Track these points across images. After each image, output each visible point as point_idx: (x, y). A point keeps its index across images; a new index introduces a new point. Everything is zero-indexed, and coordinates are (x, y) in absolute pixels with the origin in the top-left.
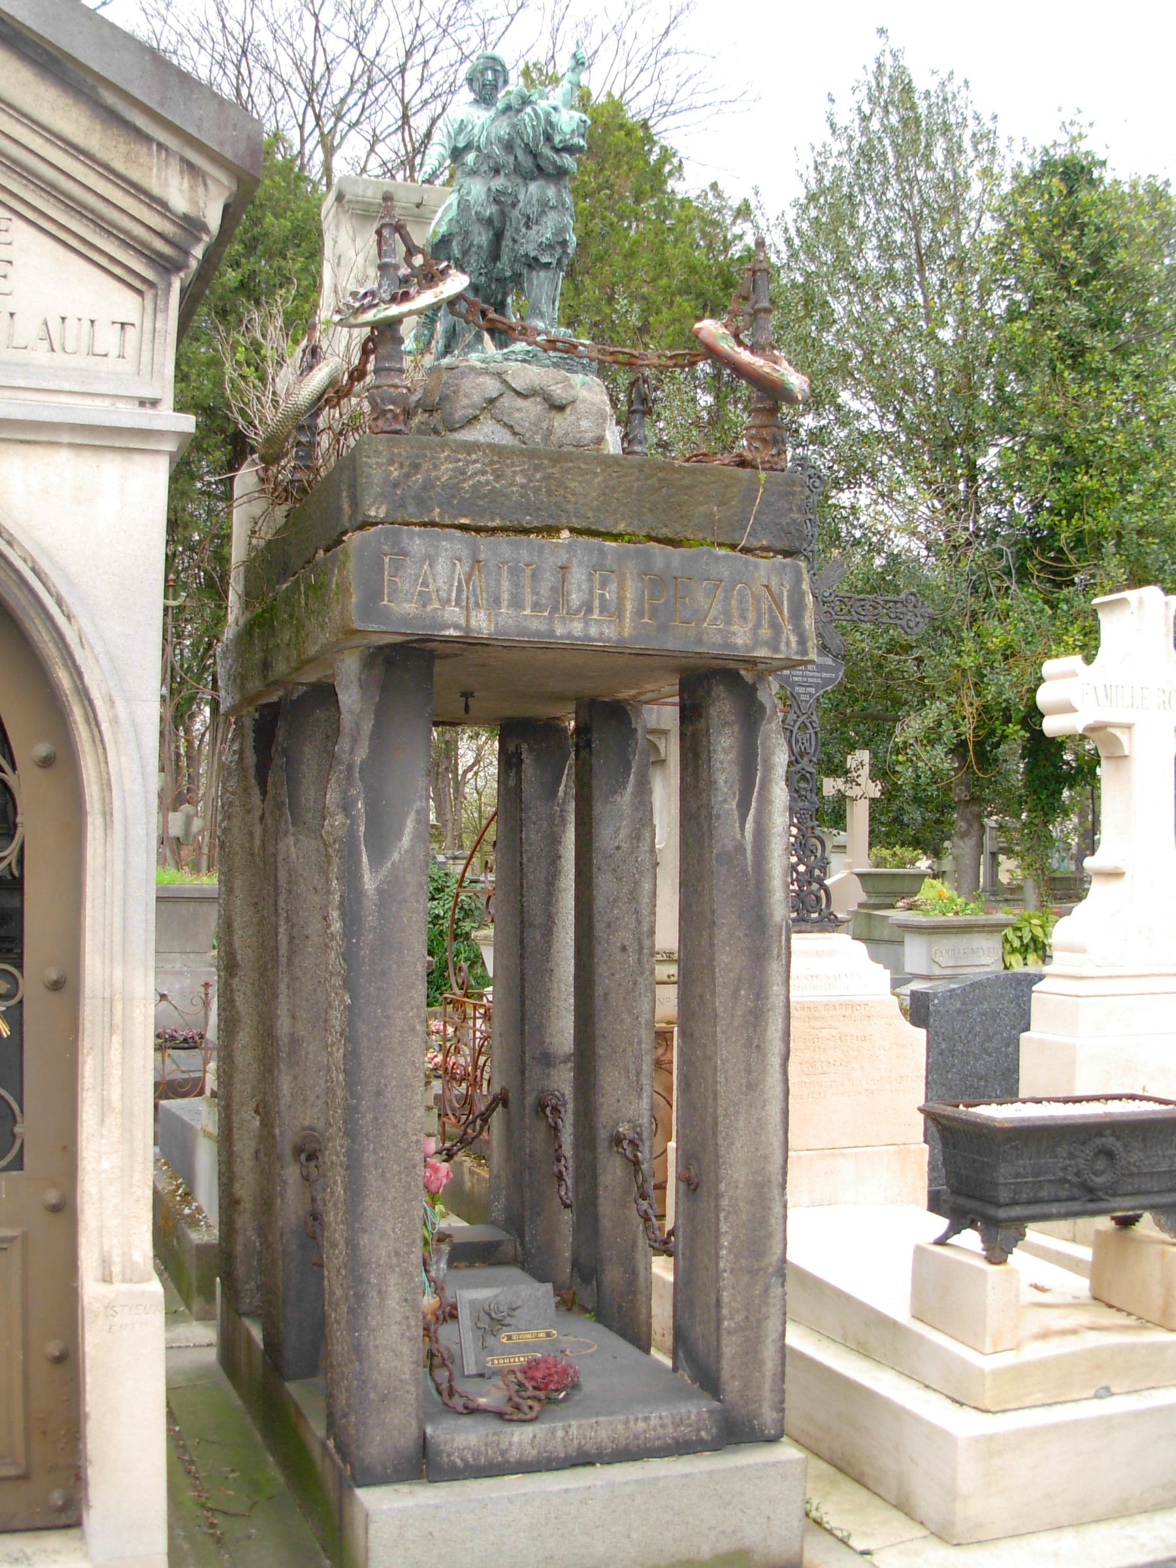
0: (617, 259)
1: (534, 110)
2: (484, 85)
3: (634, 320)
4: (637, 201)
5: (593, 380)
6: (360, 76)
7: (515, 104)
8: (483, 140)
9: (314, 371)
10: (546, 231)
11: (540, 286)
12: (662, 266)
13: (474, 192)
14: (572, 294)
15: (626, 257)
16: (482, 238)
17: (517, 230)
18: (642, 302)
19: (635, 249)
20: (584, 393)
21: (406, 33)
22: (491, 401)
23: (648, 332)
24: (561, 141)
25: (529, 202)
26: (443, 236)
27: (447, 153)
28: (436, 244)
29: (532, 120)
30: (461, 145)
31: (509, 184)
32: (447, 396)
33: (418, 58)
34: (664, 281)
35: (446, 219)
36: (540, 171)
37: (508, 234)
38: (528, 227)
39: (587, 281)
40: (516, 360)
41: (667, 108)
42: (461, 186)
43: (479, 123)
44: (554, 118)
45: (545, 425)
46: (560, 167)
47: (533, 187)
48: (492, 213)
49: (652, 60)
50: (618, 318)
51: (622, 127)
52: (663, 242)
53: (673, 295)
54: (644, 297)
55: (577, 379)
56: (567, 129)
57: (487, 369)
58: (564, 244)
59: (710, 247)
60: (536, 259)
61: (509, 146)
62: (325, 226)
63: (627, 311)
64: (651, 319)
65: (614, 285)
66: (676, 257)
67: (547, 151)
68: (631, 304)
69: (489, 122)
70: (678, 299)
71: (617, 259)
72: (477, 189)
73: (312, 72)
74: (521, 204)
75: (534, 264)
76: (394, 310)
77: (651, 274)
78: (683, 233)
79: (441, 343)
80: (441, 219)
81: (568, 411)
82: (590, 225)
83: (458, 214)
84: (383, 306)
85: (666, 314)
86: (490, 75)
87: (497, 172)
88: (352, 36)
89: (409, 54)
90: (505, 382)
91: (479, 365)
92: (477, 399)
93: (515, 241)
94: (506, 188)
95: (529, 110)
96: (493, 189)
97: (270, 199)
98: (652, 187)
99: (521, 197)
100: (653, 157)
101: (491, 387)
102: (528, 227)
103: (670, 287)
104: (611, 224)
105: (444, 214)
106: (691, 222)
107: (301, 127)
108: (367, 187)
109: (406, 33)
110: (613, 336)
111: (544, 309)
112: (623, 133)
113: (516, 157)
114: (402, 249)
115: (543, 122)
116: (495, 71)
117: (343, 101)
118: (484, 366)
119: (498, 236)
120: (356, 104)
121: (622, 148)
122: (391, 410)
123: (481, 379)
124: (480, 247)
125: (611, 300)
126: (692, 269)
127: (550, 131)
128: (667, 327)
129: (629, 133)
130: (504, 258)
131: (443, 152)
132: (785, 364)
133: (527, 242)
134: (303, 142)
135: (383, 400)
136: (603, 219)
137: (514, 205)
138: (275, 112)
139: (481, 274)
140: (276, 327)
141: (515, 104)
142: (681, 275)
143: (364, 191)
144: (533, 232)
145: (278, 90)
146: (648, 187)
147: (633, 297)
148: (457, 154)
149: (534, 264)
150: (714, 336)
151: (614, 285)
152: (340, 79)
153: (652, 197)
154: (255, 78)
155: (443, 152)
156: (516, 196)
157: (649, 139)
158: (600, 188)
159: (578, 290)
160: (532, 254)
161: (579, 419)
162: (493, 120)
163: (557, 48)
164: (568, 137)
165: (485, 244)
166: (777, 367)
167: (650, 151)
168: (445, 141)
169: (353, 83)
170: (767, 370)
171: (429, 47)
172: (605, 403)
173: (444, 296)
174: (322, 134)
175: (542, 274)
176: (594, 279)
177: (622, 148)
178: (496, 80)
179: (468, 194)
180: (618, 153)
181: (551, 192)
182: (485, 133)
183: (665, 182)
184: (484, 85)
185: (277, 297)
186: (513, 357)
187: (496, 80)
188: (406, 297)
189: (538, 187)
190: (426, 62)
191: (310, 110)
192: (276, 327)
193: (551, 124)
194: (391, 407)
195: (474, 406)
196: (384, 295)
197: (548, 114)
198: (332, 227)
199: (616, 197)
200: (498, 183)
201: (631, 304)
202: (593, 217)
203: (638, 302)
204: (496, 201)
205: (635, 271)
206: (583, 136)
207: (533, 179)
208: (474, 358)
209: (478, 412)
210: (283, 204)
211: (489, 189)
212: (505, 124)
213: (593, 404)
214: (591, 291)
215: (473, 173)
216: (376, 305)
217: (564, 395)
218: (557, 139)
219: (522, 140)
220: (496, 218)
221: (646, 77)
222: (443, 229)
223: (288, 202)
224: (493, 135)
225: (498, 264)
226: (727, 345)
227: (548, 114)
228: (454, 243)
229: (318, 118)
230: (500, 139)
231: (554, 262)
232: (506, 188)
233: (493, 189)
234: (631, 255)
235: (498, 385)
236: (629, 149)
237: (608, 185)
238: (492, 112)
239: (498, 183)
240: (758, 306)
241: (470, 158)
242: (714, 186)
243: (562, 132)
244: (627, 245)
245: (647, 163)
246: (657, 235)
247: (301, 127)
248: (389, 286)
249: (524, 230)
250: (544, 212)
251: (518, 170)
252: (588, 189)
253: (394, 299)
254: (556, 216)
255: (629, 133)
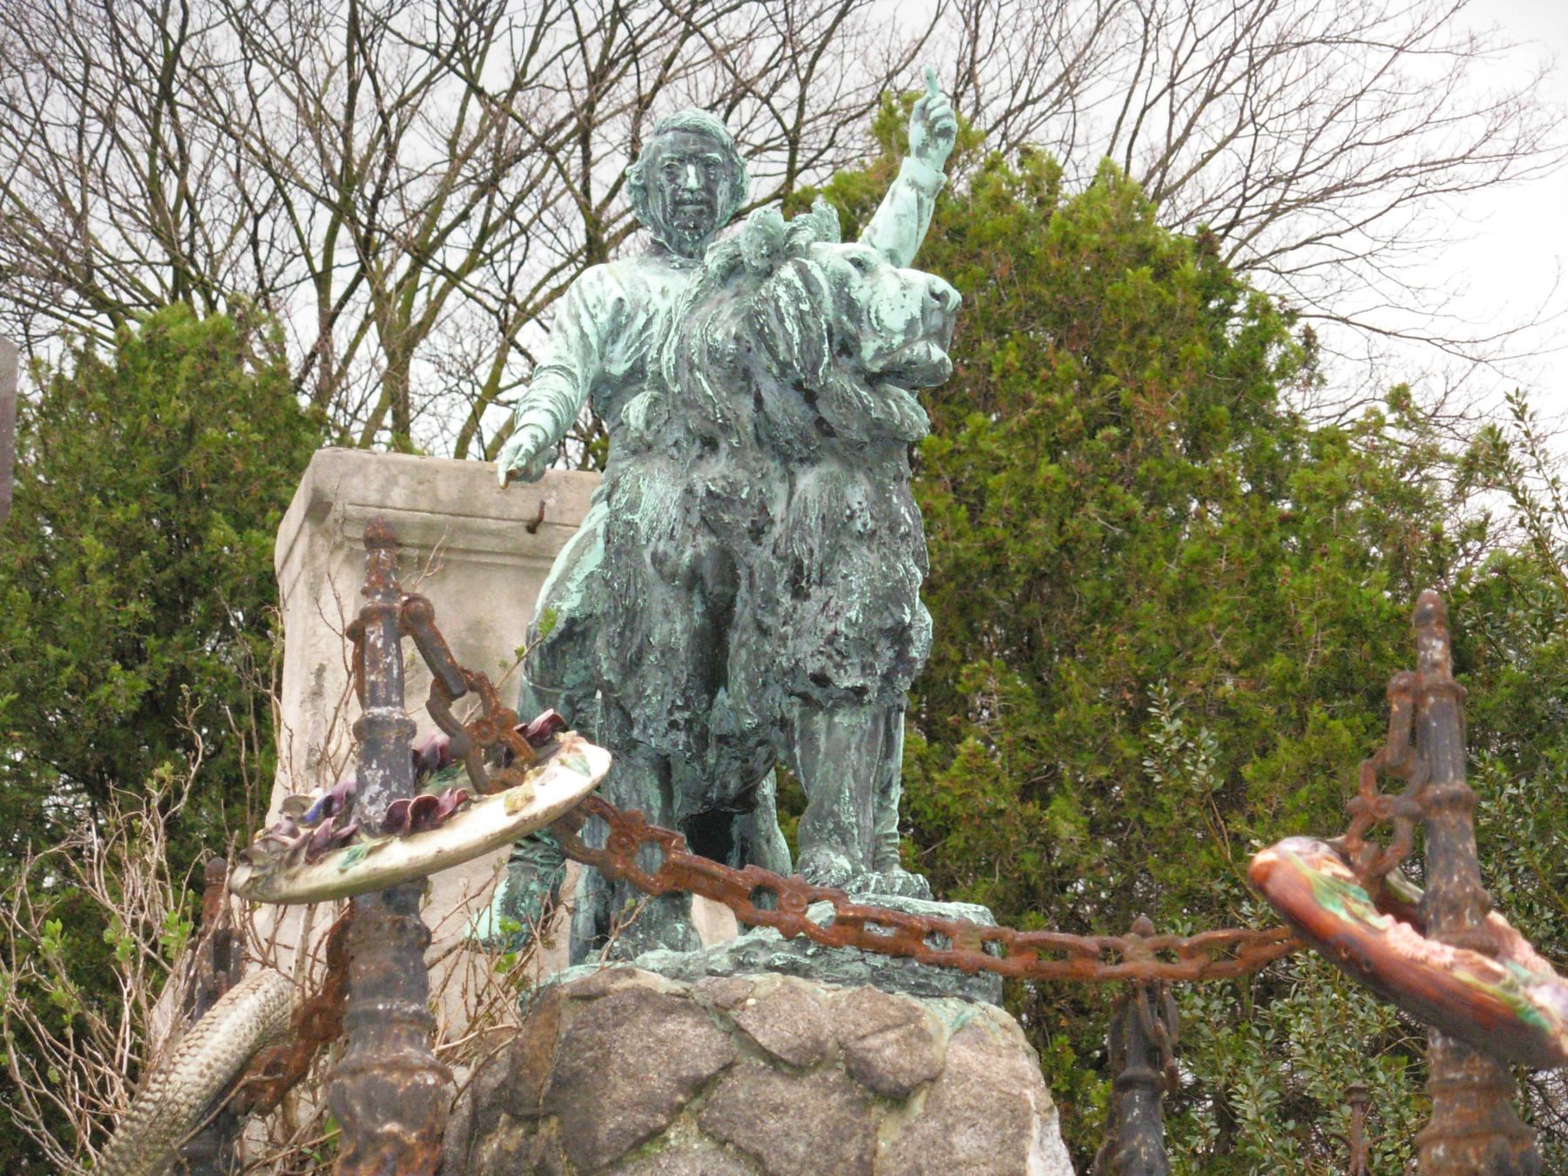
0: (1150, 611)
1: (803, 272)
2: (678, 203)
3: (1203, 773)
4: (1198, 449)
5: (991, 1015)
6: (475, 143)
7: (752, 257)
8: (669, 355)
9: (218, 1008)
10: (846, 604)
11: (837, 754)
12: (1271, 622)
13: (648, 501)
14: (1031, 709)
15: (1171, 603)
16: (673, 625)
17: (771, 602)
18: (1222, 722)
19: (1194, 580)
20: (962, 1055)
21: (588, 25)
22: (699, 1086)
23: (1239, 805)
24: (879, 353)
25: (798, 523)
26: (572, 622)
27: (578, 395)
28: (553, 646)
29: (797, 299)
30: (619, 369)
31: (741, 475)
32: (577, 1074)
33: (624, 91)
34: (1277, 665)
35: (580, 575)
36: (820, 437)
37: (743, 612)
38: (799, 594)
39: (1069, 670)
40: (770, 967)
41: (1280, 193)
42: (614, 486)
43: (663, 306)
44: (860, 289)
45: (851, 1150)
46: (878, 424)
47: (808, 481)
48: (697, 558)
49: (1239, 64)
50: (1161, 770)
51: (1144, 253)
52: (1269, 557)
53: (1304, 698)
54: (1226, 711)
55: (942, 1014)
56: (895, 320)
57: (685, 996)
58: (900, 635)
59: (1399, 565)
60: (821, 680)
61: (739, 374)
62: (284, 583)
63: (1183, 748)
64: (1248, 771)
65: (1143, 682)
66: (1305, 598)
67: (843, 382)
68: (1192, 730)
69: (683, 308)
70: (1316, 712)
71: (1150, 611)
72: (657, 493)
73: (347, 135)
74: (778, 529)
75: (817, 693)
76: (399, 854)
77: (1243, 647)
78: (1322, 529)
79: (584, 921)
80: (566, 576)
81: (918, 1105)
82: (1072, 524)
83: (606, 564)
84: (366, 842)
85: (1286, 754)
86: (691, 177)
87: (710, 444)
88: (450, 36)
89: (598, 79)
90: (739, 1030)
91: (663, 985)
92: (657, 1081)
93: (764, 631)
94: (734, 487)
95: (788, 271)
96: (700, 490)
97: (222, 476)
98: (1234, 409)
99: (777, 510)
100: (1233, 329)
101: (698, 1043)
102: (799, 594)
103: (1294, 678)
104: (1128, 518)
105: (574, 562)
106: (1342, 499)
107: (322, 281)
108: (392, 481)
109: (588, 25)
110: (1148, 817)
111: (848, 819)
112: (1146, 270)
113: (759, 401)
114: (422, 682)
115: (828, 304)
116: (707, 164)
117: (435, 205)
118: (678, 986)
119: (719, 619)
120: (465, 216)
121: (1149, 312)
122: (393, 1137)
123: (670, 1026)
124: (668, 650)
125: (1138, 719)
126: (1353, 628)
127: (851, 327)
128: (1293, 790)
129: (1162, 272)
130: (738, 679)
131: (568, 390)
132: (1524, 949)
133: (798, 634)
134: (328, 320)
135: (370, 1105)
136: (1107, 504)
137: (757, 533)
138: (254, 242)
139: (673, 725)
140: (145, 868)
141: (752, 257)
142: (1321, 645)
143: (384, 491)
144: (812, 606)
145: (261, 188)
146: (1223, 410)
147: (1200, 710)
148: (606, 393)
149: (817, 693)
150: (1309, 888)
151: (1143, 682)
152: (420, 149)
153: (1237, 435)
154: (197, 153)
155: (568, 390)
156: (763, 509)
157: (1219, 282)
158: (1093, 425)
159: (1048, 698)
160: (812, 666)
161: (948, 1129)
162: (695, 302)
163: (982, 47)
164: (898, 340)
165: (681, 641)
166: (1495, 966)
167: (1225, 312)
168: (573, 359)
169: (457, 159)
170: (1464, 975)
171: (650, 64)
172: (1022, 1079)
173: (538, 808)
174: (378, 295)
175: (842, 719)
176: (1089, 665)
177: (1149, 312)
178: (709, 188)
179: (633, 506)
180: (1136, 327)
181: (858, 495)
182: (674, 339)
183: (1271, 393)
184: (678, 203)
185: (151, 786)
186: (762, 958)
187: (709, 188)
188: (427, 816)
189: (822, 479)
190: (643, 103)
191: (344, 233)
192: (145, 868)
193: (850, 307)
194: (392, 1127)
195: (649, 1104)
196: (371, 810)
197: (841, 283)
198: (301, 589)
199: (1140, 442)
200: (715, 472)
201: (1192, 730)
202: (1080, 501)
203: (1210, 724)
204: (710, 525)
205: (1199, 639)
206: (939, 336)
207: (810, 460)
208: (653, 967)
209: (661, 1120)
210: (257, 489)
211: (690, 491)
212: (727, 309)
213: (987, 1084)
214: (1085, 696)
215: (642, 449)
216: (346, 841)
217: (905, 1062)
218: (869, 348)
219: (772, 351)
220: (708, 570)
221: (1219, 118)
222: (571, 603)
223: (271, 483)
224: (694, 342)
225: (721, 695)
226: (1346, 910)
227: (841, 283)
228: (600, 642)
229: (366, 247)
230: (714, 355)
231: (873, 684)
232: (734, 487)
233: (700, 490)
234: (1185, 597)
235: (718, 1040)
236: (1166, 314)
237: (1117, 413)
238: (697, 275)
239: (715, 472)
240: (1436, 790)
241: (636, 409)
242: (1399, 398)
243: (880, 329)
244: (1174, 571)
245: (1217, 343)
246: (1250, 537)
247: (322, 281)
248: (385, 783)
249: (786, 600)
250: (837, 548)
251: (765, 437)
252: (1062, 429)
253: (398, 824)
254: (873, 559)
255: (1162, 272)
